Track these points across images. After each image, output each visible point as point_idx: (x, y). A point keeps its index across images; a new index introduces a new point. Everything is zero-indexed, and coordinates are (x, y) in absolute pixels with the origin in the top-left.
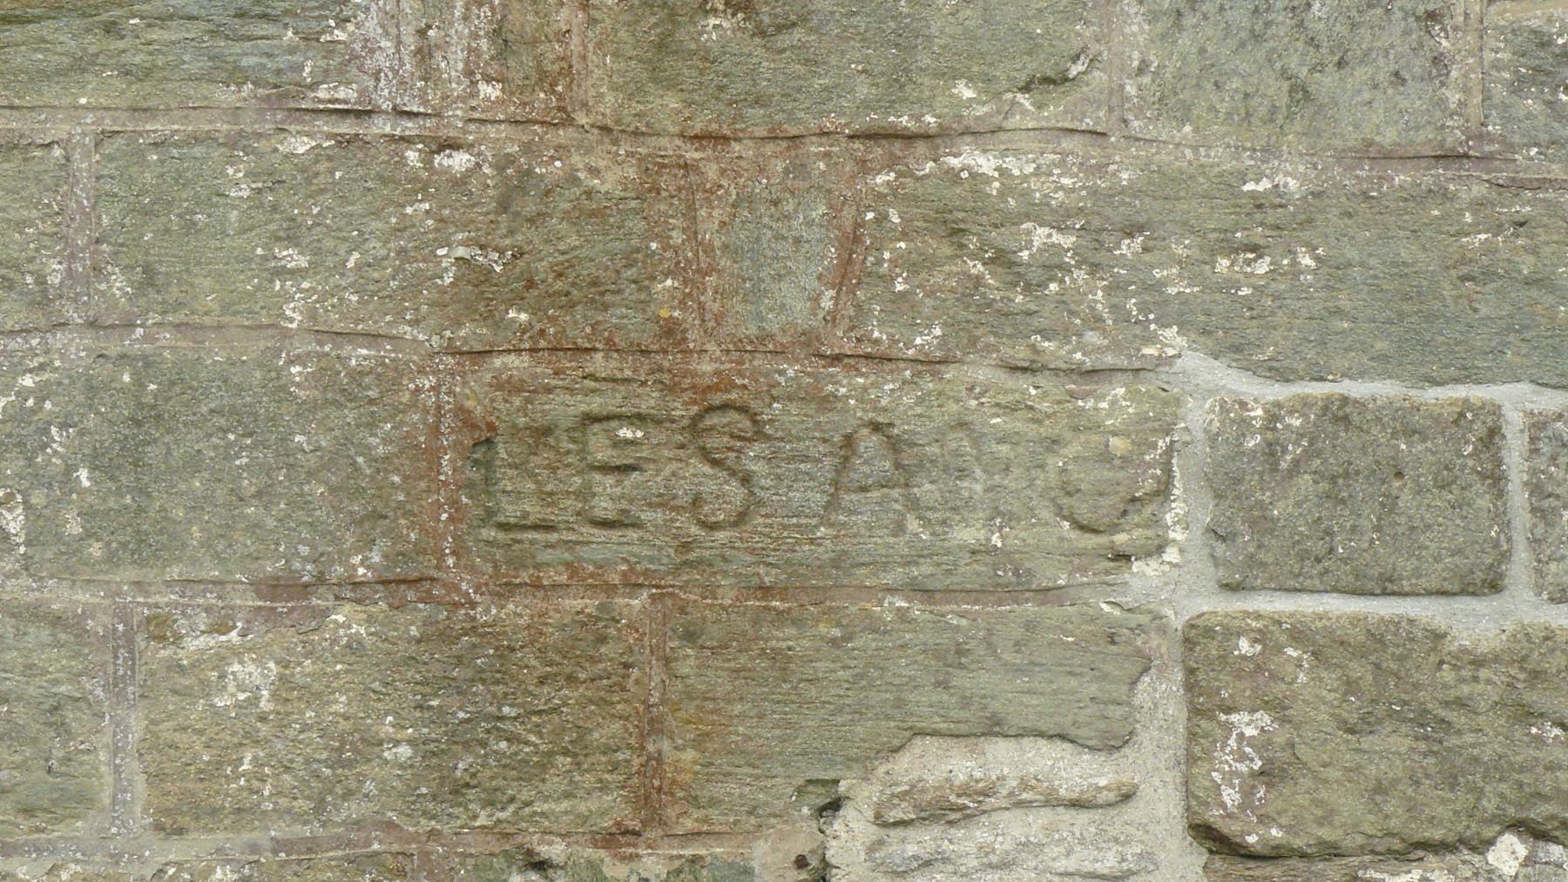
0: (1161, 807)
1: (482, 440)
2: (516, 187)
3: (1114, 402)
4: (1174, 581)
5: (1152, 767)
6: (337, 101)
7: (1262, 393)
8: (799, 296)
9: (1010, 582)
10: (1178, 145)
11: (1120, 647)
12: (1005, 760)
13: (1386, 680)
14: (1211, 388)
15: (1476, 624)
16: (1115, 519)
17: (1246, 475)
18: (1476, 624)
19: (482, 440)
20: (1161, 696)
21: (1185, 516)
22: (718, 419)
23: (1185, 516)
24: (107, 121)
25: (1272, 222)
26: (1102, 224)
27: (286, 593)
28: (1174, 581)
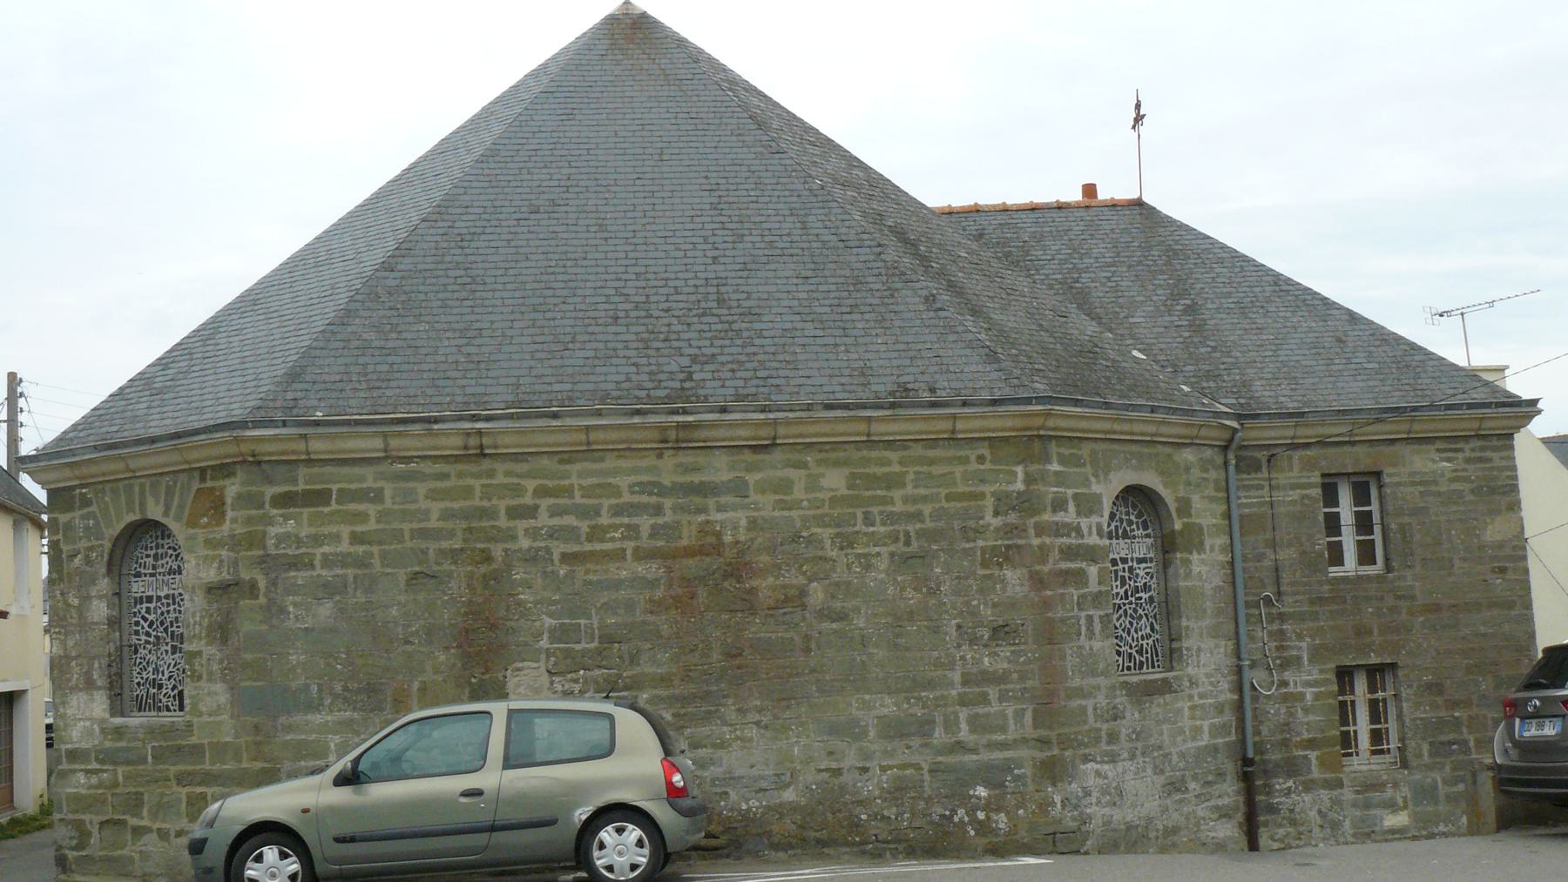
0: (543, 669)
1: (467, 631)
2: (470, 602)
3: (538, 624)
4: (544, 643)
5: (542, 664)
6: (1115, 432)
7: (554, 622)
8: (502, 613)
9: (526, 644)
10: (547, 594)
11: (539, 651)
12: (526, 664)
13: (568, 653)
14: (549, 622)
15: (578, 647)
16: (538, 636)
17: (552, 631)
18: (578, 647)
19: (467, 631)
20: (543, 656)
21: (546, 636)
22: (493, 627)
23: (546, 636)
24: (645, 532)
25: (555, 602)
26: (536, 603)
27: (447, 648)
28: (544, 643)
